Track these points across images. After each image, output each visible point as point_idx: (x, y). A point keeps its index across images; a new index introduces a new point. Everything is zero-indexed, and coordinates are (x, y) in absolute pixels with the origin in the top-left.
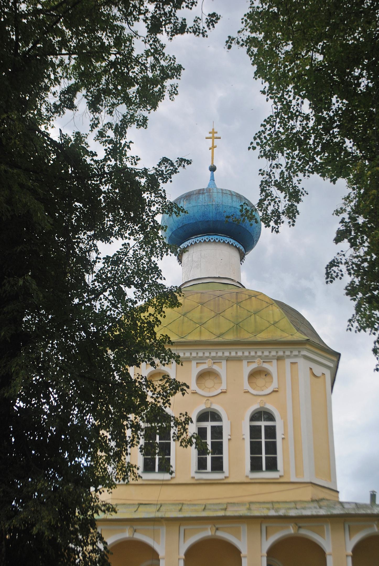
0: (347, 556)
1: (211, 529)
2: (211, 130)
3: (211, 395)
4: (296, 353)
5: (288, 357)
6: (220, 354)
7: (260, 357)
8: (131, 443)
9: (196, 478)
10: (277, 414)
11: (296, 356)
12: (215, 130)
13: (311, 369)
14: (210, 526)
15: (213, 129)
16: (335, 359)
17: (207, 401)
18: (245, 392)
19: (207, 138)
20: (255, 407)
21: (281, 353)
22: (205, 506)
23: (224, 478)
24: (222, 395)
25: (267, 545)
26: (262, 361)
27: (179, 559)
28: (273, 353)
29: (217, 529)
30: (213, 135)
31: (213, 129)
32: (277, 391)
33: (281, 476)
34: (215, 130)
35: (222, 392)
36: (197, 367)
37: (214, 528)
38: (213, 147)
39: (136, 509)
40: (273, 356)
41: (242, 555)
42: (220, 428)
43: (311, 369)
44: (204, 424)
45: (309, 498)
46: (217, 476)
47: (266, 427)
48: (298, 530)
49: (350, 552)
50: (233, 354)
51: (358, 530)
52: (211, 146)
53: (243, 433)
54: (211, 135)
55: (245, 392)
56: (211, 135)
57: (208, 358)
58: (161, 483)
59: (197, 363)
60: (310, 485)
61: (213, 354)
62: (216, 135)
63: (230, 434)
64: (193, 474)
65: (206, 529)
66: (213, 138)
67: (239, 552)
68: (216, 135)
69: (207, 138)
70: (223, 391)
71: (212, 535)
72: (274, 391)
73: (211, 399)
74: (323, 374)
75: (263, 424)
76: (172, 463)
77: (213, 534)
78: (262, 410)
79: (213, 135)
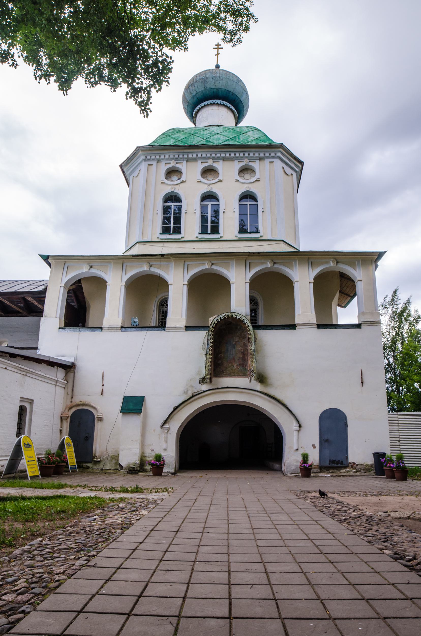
0: (310, 282)
1: (208, 264)
2: (217, 44)
4: (273, 155)
5: (267, 157)
6: (218, 155)
7: (247, 157)
9: (199, 237)
11: (273, 157)
12: (219, 44)
13: (283, 168)
14: (207, 262)
15: (218, 43)
16: (300, 166)
17: (208, 187)
18: (236, 181)
19: (214, 48)
21: (262, 155)
26: (248, 160)
27: (183, 285)
28: (257, 155)
29: (212, 264)
30: (218, 47)
31: (218, 43)
32: (259, 181)
34: (219, 44)
35: (219, 181)
37: (210, 264)
38: (218, 54)
40: (257, 157)
43: (283, 168)
44: (205, 203)
48: (274, 265)
50: (228, 155)
51: (319, 264)
52: (216, 53)
53: (214, 68)
54: (217, 47)
55: (236, 181)
56: (217, 47)
57: (209, 158)
59: (202, 162)
61: (213, 155)
62: (220, 47)
64: (197, 235)
65: (204, 264)
66: (218, 48)
68: (220, 47)
69: (214, 48)
71: (208, 269)
72: (256, 181)
74: (291, 174)
77: (210, 267)
78: (249, 194)
79: (218, 47)
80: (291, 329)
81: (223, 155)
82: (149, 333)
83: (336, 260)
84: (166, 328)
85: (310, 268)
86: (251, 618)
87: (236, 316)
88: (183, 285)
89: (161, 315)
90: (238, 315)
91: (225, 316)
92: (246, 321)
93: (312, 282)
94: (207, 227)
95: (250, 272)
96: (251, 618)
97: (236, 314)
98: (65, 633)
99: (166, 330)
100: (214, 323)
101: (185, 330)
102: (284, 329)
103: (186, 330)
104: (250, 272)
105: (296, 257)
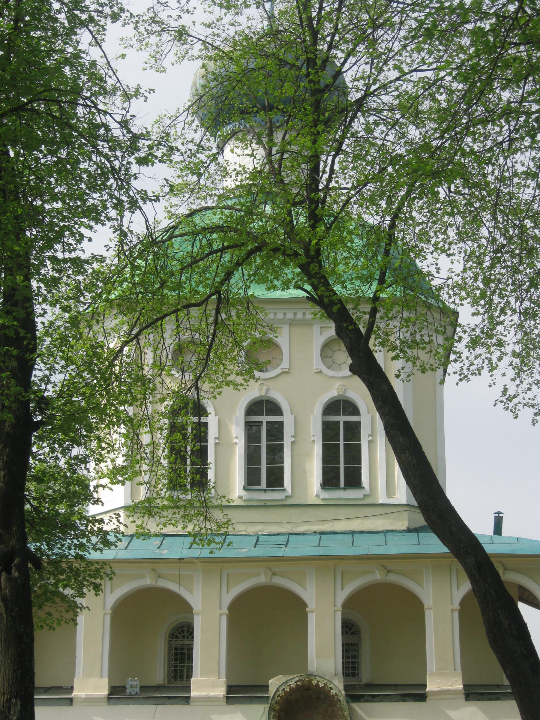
1: (265, 573)
3: (266, 378)
8: (40, 452)
10: (284, 406)
20: (332, 393)
22: (258, 538)
23: (362, 497)
24: (283, 378)
25: (228, 598)
27: (220, 614)
33: (365, 496)
36: (321, 334)
39: (159, 543)
41: (307, 609)
42: (358, 424)
45: (404, 528)
46: (275, 496)
47: (346, 423)
48: (386, 575)
49: (457, 606)
50: (300, 316)
55: (316, 373)
58: (262, 503)
60: (405, 508)
63: (293, 434)
67: (305, 605)
70: (284, 370)
73: (266, 383)
75: (342, 419)
76: (211, 475)
80: (416, 701)
81: (290, 316)
82: (160, 707)
83: (503, 566)
84: (191, 700)
85: (454, 577)
86: (220, 598)
87: (318, 682)
88: (220, 614)
89: (173, 657)
90: (321, 680)
91: (298, 681)
92: (334, 691)
93: (456, 610)
94: (259, 470)
95: (342, 590)
96: (220, 598)
97: (318, 679)
98: (523, 607)
99: (192, 703)
100: (279, 696)
101: (225, 703)
102: (404, 701)
103: (227, 703)
104: (342, 590)
105: (428, 560)
